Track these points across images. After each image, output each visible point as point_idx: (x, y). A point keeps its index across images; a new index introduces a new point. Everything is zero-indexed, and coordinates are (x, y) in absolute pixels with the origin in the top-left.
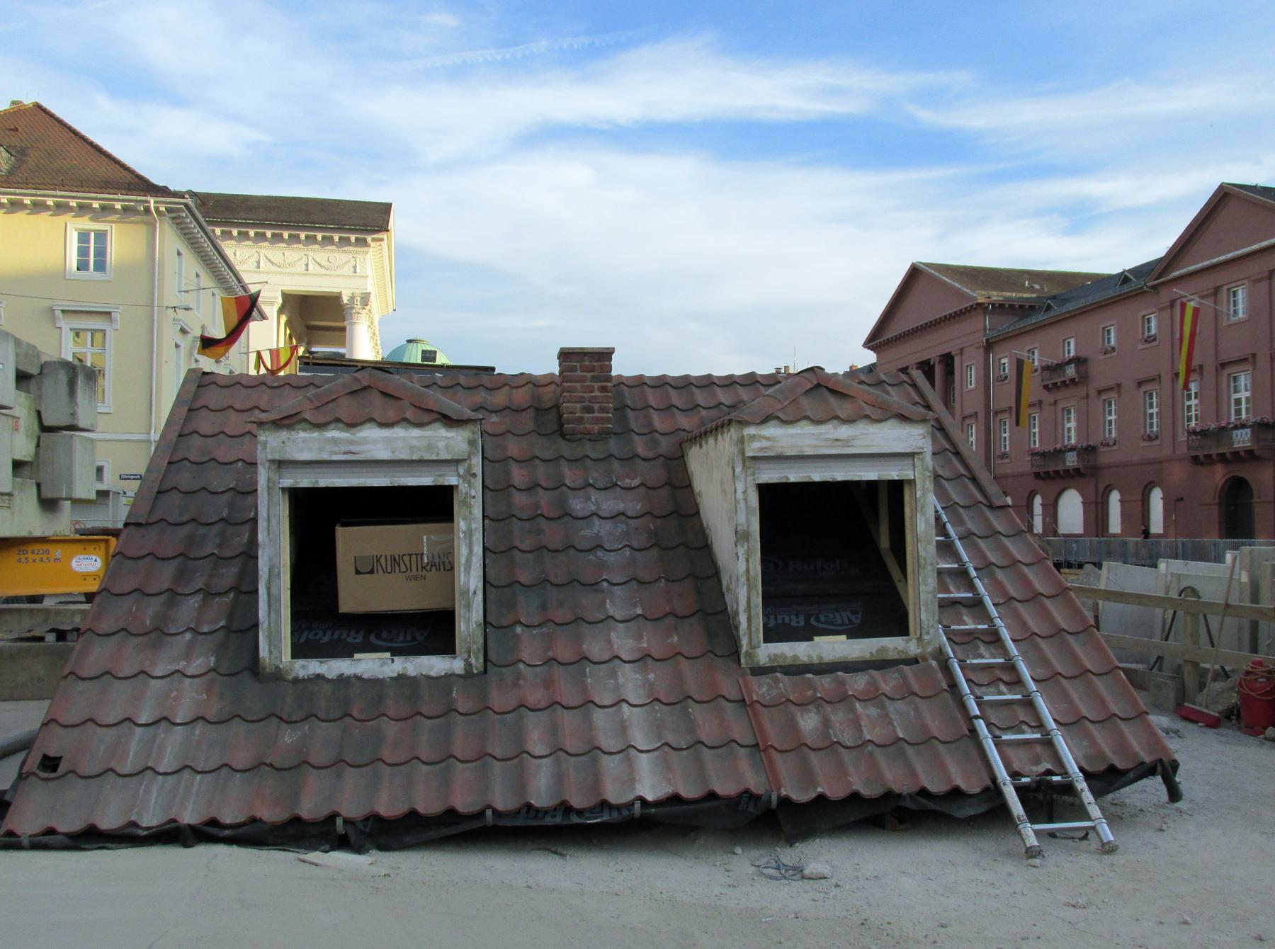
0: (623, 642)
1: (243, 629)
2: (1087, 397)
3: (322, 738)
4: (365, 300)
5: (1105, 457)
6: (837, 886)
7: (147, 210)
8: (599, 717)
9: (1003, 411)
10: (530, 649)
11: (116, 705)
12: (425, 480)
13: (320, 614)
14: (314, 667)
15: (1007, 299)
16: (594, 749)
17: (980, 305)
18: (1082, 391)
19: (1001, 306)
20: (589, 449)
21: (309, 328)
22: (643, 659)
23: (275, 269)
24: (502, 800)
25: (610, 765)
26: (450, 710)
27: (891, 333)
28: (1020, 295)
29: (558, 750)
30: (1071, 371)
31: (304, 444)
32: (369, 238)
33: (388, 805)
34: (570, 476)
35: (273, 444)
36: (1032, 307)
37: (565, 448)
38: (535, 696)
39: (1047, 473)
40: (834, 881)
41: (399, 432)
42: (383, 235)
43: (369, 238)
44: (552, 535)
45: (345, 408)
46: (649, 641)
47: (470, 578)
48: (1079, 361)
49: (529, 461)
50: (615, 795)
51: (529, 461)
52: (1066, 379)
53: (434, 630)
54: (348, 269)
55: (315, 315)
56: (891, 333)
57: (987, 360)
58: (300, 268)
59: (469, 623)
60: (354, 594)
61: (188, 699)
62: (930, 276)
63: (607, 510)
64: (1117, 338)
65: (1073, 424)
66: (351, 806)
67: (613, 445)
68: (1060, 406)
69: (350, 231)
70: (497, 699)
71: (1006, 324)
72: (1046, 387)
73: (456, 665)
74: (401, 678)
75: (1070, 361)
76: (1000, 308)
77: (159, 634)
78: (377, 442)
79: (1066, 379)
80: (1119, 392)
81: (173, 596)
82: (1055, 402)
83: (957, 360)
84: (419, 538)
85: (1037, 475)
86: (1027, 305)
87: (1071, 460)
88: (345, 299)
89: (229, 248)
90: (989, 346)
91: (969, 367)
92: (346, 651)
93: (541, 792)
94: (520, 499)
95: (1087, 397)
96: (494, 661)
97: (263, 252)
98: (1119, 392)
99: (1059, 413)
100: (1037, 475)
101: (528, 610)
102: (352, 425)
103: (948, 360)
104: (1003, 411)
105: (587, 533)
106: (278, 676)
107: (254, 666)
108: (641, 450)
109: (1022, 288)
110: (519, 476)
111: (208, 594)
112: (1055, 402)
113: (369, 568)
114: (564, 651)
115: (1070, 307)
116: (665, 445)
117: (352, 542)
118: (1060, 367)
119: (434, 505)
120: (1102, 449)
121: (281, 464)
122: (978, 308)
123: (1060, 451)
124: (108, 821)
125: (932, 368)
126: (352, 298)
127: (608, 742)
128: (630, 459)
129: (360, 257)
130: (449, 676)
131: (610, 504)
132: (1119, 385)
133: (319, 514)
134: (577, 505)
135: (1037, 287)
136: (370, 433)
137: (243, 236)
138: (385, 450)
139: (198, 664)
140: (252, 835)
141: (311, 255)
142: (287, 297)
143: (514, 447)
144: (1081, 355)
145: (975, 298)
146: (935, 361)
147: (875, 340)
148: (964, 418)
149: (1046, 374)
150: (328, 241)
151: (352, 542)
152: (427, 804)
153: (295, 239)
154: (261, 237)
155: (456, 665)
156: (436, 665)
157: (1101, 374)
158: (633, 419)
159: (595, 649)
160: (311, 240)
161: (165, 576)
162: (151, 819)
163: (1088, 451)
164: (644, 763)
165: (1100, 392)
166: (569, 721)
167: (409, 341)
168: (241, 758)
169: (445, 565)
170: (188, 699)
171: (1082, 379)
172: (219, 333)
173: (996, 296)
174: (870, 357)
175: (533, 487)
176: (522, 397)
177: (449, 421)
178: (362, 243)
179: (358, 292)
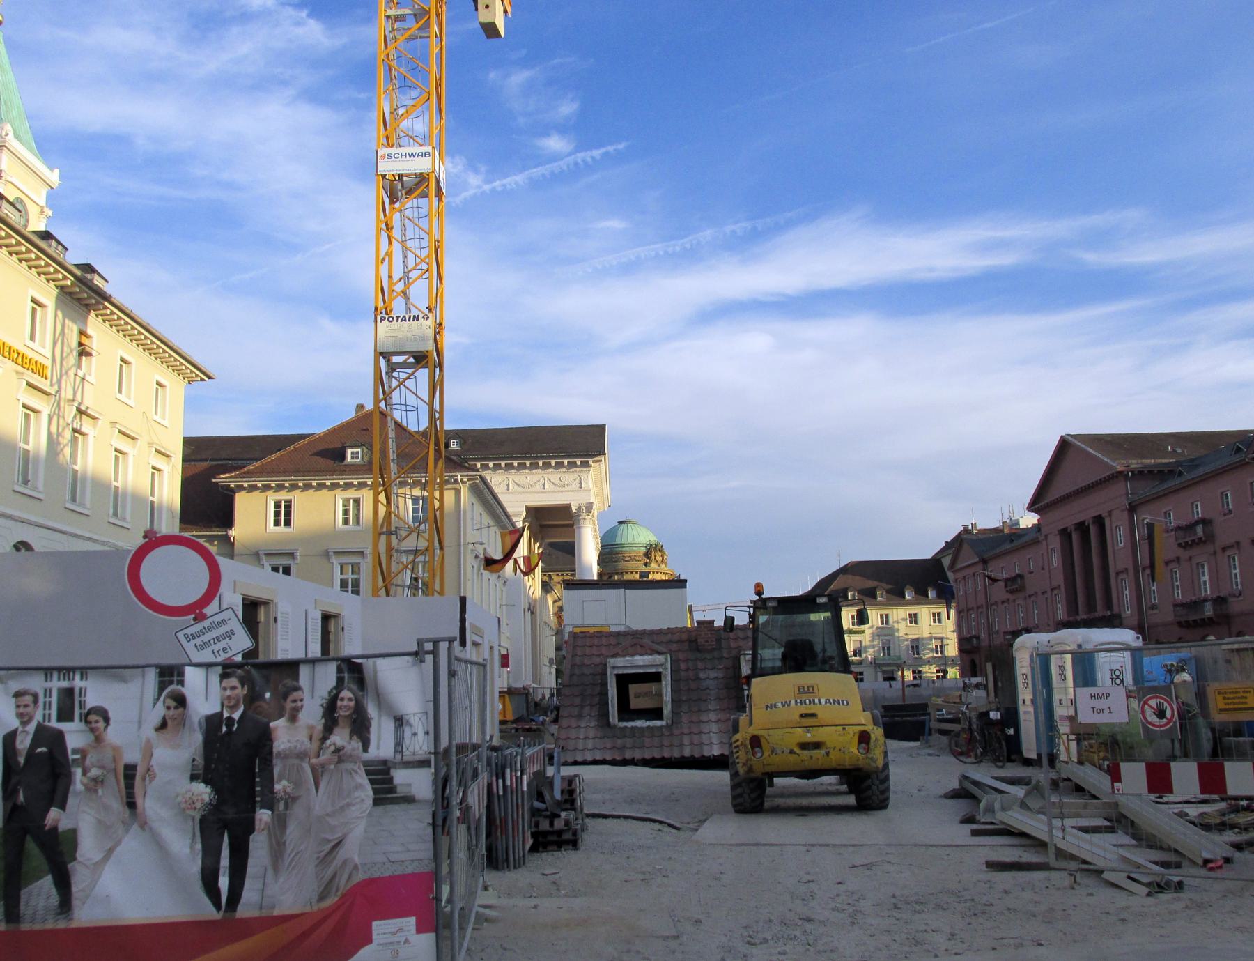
0: (713, 716)
1: (604, 715)
2: (1215, 553)
3: (629, 742)
4: (589, 508)
5: (1236, 606)
6: (894, 896)
7: (456, 482)
8: (704, 737)
9: (1231, 546)
10: (685, 718)
11: (573, 734)
12: (653, 670)
13: (626, 711)
14: (625, 724)
15: (1146, 466)
16: (702, 744)
17: (1120, 473)
18: (1210, 548)
19: (1141, 472)
20: (708, 656)
21: (542, 526)
22: (718, 721)
23: (520, 489)
24: (676, 754)
25: (706, 747)
26: (662, 735)
27: (1053, 494)
28: (1159, 461)
29: (692, 744)
30: (1199, 530)
31: (620, 661)
32: (590, 461)
33: (648, 756)
34: (700, 665)
35: (612, 661)
36: (1171, 472)
37: (699, 655)
38: (686, 731)
39: (1187, 622)
40: (894, 901)
41: (645, 657)
42: (602, 458)
43: (590, 461)
44: (693, 685)
45: (630, 650)
46: (722, 716)
47: (667, 698)
48: (1205, 522)
49: (686, 661)
50: (706, 754)
51: (686, 661)
52: (1197, 536)
53: (656, 713)
54: (575, 486)
55: (554, 526)
56: (1053, 494)
57: (1132, 522)
58: (539, 487)
59: (667, 711)
60: (635, 704)
61: (592, 733)
62: (1078, 448)
63: (712, 676)
64: (1233, 501)
65: (1206, 578)
66: (638, 755)
67: (716, 654)
68: (1195, 561)
69: (577, 457)
70: (676, 732)
71: (1147, 488)
72: (1180, 545)
73: (664, 723)
74: (648, 727)
75: (1197, 522)
76: (1140, 474)
77: (580, 716)
78: (640, 660)
79: (1197, 536)
80: (1239, 549)
81: (582, 706)
82: (1190, 558)
83: (1107, 522)
84: (653, 687)
85: (1180, 624)
86: (1166, 470)
87: (1209, 610)
88: (574, 509)
89: (488, 475)
90: (1132, 509)
91: (1118, 527)
92: (633, 720)
93: (687, 753)
94: (683, 674)
95: (1215, 553)
96: (674, 722)
97: (511, 477)
98: (1239, 549)
99: (1194, 566)
100: (1180, 624)
101: (685, 708)
102: (632, 655)
103: (1099, 521)
104: (1231, 546)
105: (704, 684)
106: (615, 726)
107: (608, 724)
108: (725, 655)
109: (1165, 454)
110: (683, 666)
111: (592, 706)
112: (1190, 558)
113: (639, 697)
114: (695, 719)
115: (1201, 471)
116: (734, 652)
117: (633, 689)
118: (1191, 527)
119: (656, 677)
120: (1231, 599)
121: (614, 667)
122: (1118, 476)
123: (1195, 602)
124: (579, 759)
125: (1070, 536)
126: (579, 508)
127: (707, 742)
128: (722, 658)
129: (584, 476)
130: (662, 727)
131: (712, 674)
132: (1238, 543)
133: (624, 681)
134: (702, 675)
135: (1179, 451)
136: (638, 657)
137: (497, 467)
138: (642, 662)
139: (593, 724)
140: (613, 763)
141: (547, 476)
142: (528, 509)
143: (681, 656)
144: (1207, 517)
145: (1114, 467)
146: (1089, 522)
147: (1034, 506)
148: (1117, 574)
149: (1181, 533)
150: (559, 465)
151: (633, 689)
152: (657, 756)
153: (534, 466)
154: (509, 467)
155: (664, 723)
156: (658, 723)
157: (1224, 535)
158: (724, 643)
159: (704, 718)
160: (547, 466)
161: (577, 701)
162: (589, 759)
163: (1220, 601)
164: (715, 747)
165: (1224, 549)
166: (695, 737)
167: (620, 523)
168: (609, 746)
169: (660, 695)
170: (592, 733)
171: (1209, 538)
172: (498, 555)
173: (1135, 463)
174: (1030, 520)
175: (687, 670)
176: (684, 637)
177: (659, 653)
178: (585, 465)
179: (584, 502)
